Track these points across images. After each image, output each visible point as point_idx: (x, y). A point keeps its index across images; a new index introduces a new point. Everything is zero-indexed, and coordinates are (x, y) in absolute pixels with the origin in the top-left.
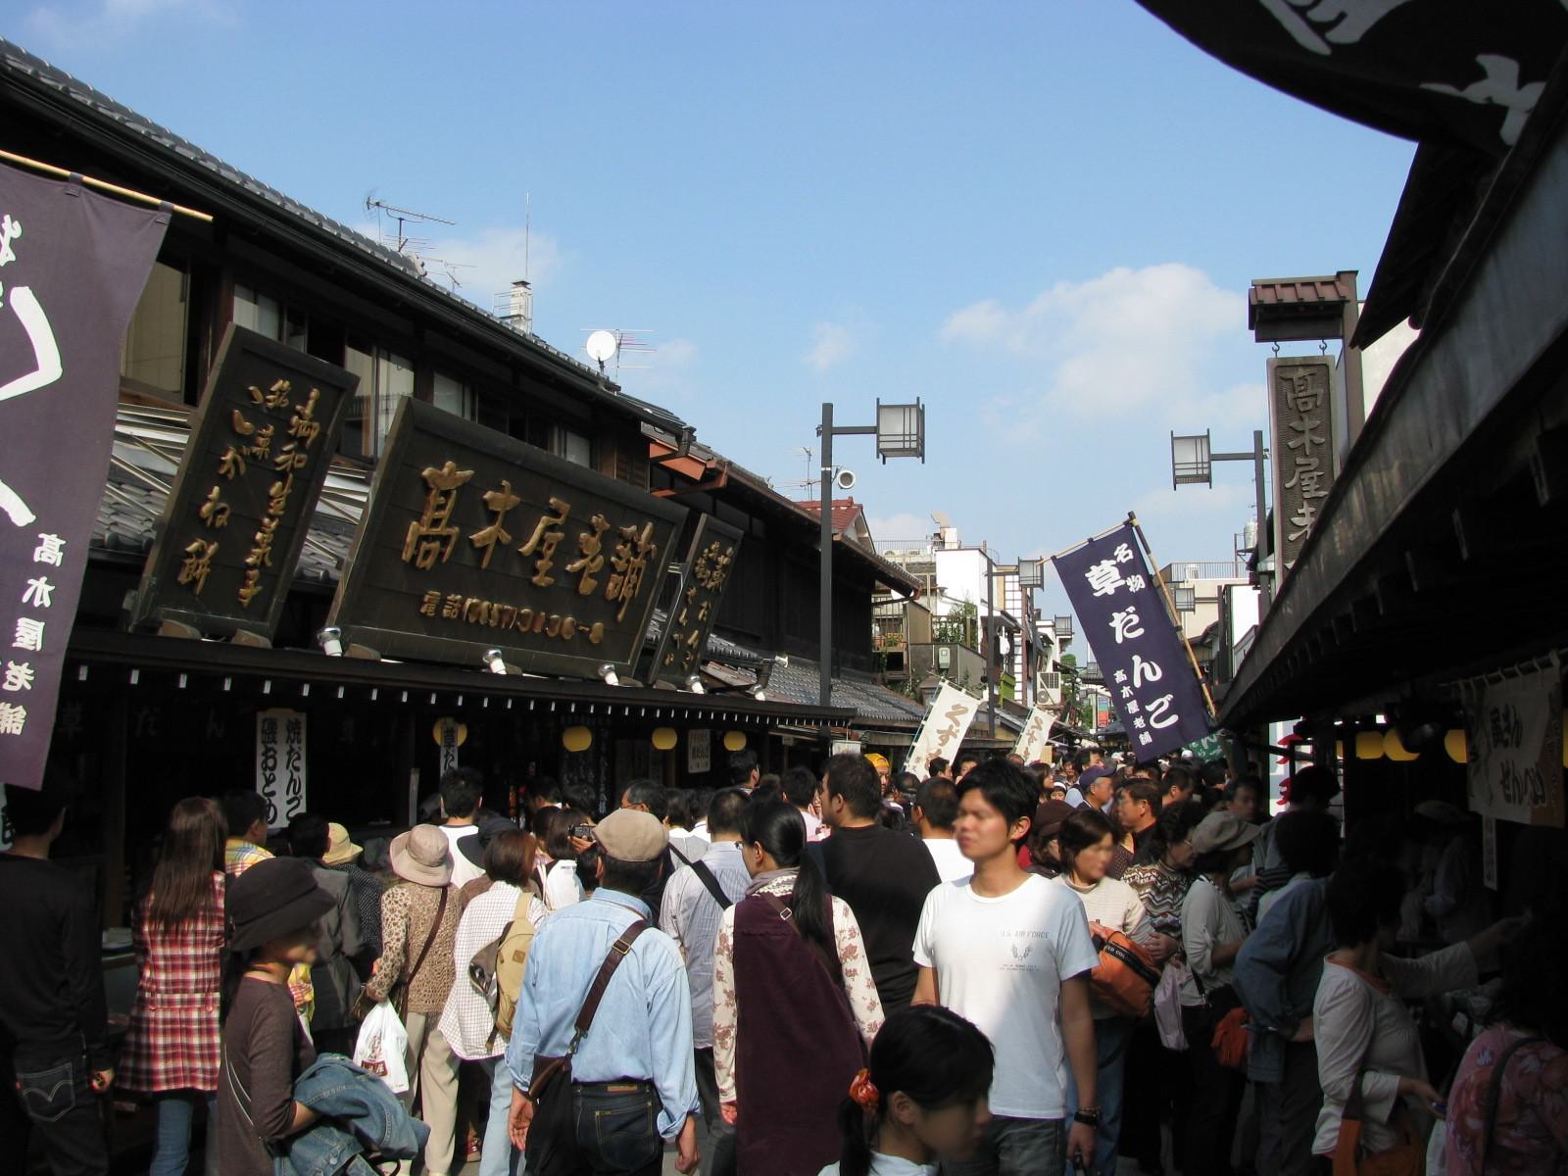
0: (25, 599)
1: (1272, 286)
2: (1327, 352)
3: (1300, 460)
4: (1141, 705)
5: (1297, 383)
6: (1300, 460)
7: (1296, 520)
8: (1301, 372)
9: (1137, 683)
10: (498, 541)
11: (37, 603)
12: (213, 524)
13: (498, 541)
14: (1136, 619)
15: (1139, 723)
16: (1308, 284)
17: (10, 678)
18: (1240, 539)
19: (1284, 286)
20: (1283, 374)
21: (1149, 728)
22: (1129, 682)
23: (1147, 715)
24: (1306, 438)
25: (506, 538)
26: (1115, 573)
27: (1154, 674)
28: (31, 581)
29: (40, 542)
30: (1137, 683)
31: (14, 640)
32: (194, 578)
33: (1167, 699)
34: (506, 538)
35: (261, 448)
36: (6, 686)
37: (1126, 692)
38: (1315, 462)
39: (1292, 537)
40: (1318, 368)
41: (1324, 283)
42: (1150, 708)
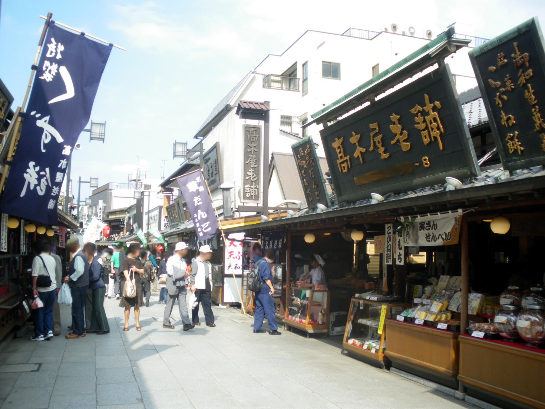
0: (59, 166)
1: (252, 103)
2: (260, 124)
3: (250, 155)
4: (200, 225)
5: (251, 132)
6: (250, 155)
7: (248, 173)
8: (252, 129)
9: (199, 218)
10: (361, 152)
11: (63, 168)
12: (508, 125)
13: (361, 152)
14: (200, 199)
15: (199, 230)
16: (256, 103)
17: (53, 191)
18: (130, 176)
19: (255, 103)
20: (247, 129)
21: (202, 231)
22: (197, 217)
23: (202, 228)
24: (253, 149)
25: (364, 150)
26: (196, 185)
27: (204, 215)
28: (61, 161)
29: (64, 148)
30: (199, 218)
31: (55, 179)
32: (514, 149)
33: (208, 223)
34: (364, 150)
35: (510, 85)
36: (52, 194)
37: (196, 220)
38: (254, 156)
39: (247, 178)
40: (257, 129)
41: (261, 104)
42: (203, 226)
